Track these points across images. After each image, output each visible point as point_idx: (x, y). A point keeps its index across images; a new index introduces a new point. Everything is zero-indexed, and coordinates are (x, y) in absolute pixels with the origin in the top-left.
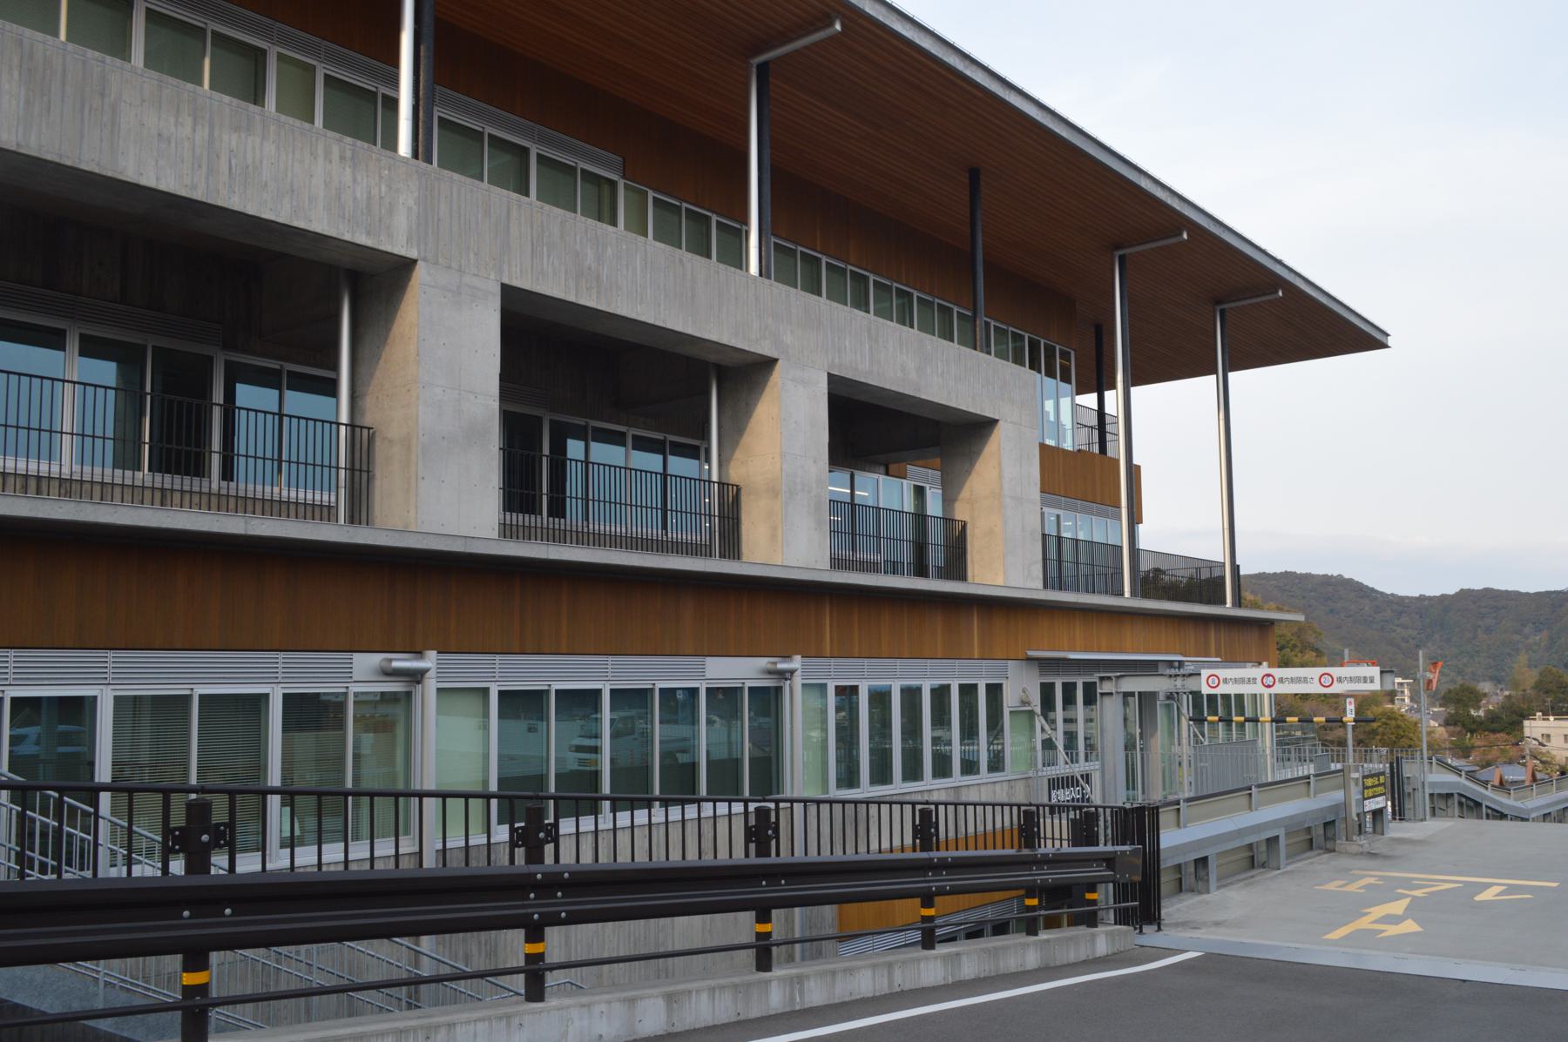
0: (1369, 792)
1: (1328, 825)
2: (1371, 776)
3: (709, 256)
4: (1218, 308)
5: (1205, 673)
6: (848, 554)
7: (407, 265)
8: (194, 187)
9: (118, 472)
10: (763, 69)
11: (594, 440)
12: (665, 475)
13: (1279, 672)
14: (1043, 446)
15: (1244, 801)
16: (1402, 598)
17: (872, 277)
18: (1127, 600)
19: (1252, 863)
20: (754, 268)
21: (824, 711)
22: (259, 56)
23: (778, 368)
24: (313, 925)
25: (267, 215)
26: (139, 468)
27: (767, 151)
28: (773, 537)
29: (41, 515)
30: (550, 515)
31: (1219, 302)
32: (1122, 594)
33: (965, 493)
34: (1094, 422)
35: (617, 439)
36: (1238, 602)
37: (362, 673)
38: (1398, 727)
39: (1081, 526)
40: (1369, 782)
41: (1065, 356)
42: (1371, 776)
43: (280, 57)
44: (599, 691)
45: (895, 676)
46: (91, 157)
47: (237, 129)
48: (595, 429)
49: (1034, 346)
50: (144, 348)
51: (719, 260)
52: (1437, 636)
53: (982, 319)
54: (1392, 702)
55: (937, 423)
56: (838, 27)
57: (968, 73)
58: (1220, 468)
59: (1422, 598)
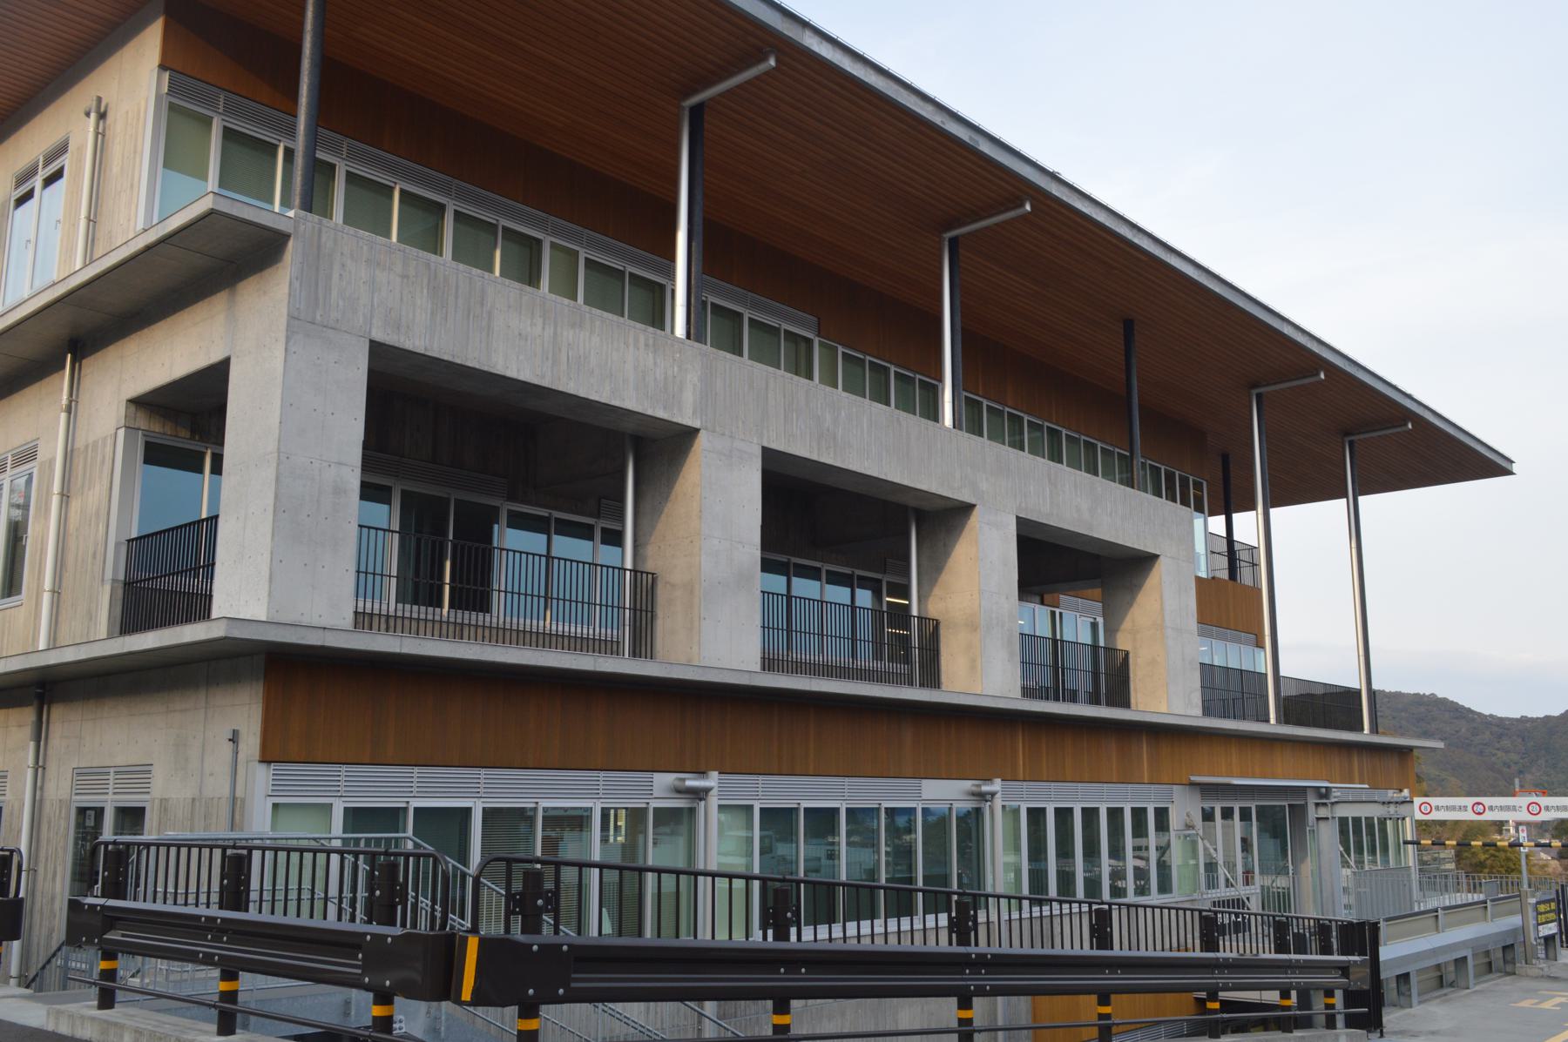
0: (1542, 918)
1: (1507, 948)
2: (1544, 902)
3: (741, 354)
4: (1347, 439)
5: (1418, 801)
6: (782, 651)
7: (692, 433)
8: (543, 377)
9: (400, 606)
10: (697, 112)
11: (797, 575)
12: (789, 597)
13: (1545, 801)
14: (1198, 579)
15: (1431, 922)
16: (1502, 719)
17: (1026, 418)
18: (1273, 726)
19: (1441, 982)
20: (680, 330)
21: (750, 840)
22: (441, 208)
23: (976, 512)
24: (1197, 934)
25: (594, 397)
26: (440, 605)
27: (699, 197)
28: (973, 667)
29: (675, 676)
30: (451, 606)
31: (1347, 434)
32: (1267, 721)
33: (1127, 624)
34: (1224, 548)
35: (813, 574)
36: (1375, 729)
37: (660, 788)
38: (1508, 859)
39: (1232, 655)
40: (1542, 908)
41: (1198, 486)
42: (1544, 902)
43: (553, 245)
44: (468, 811)
45: (1077, 797)
46: (473, 358)
47: (573, 326)
48: (860, 578)
49: (1170, 478)
50: (448, 500)
51: (897, 407)
52: (1542, 762)
53: (1139, 460)
54: (1500, 832)
55: (1097, 557)
56: (1028, 207)
57: (1136, 241)
58: (1349, 591)
59: (1524, 720)
